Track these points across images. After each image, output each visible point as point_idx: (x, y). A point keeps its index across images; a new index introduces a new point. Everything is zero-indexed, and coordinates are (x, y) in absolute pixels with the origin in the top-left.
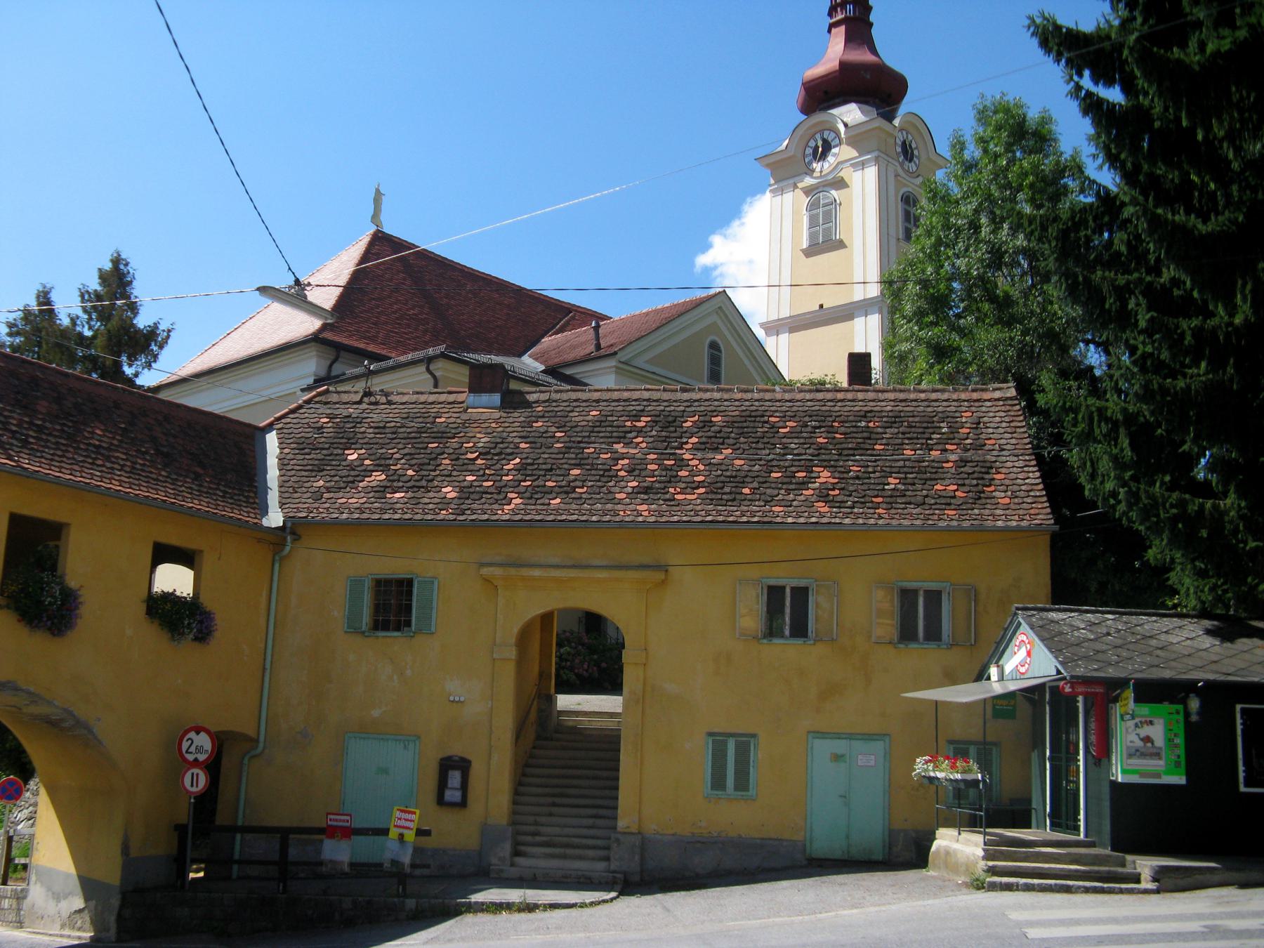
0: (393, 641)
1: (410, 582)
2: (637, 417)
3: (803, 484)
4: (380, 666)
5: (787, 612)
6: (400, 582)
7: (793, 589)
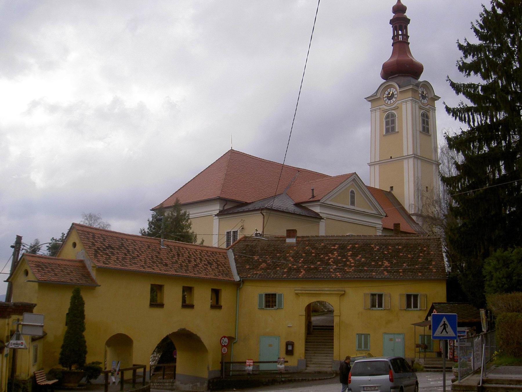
0: (271, 312)
1: (275, 294)
2: (334, 246)
3: (381, 266)
4: (269, 317)
5: (377, 301)
6: (273, 294)
7: (375, 307)
